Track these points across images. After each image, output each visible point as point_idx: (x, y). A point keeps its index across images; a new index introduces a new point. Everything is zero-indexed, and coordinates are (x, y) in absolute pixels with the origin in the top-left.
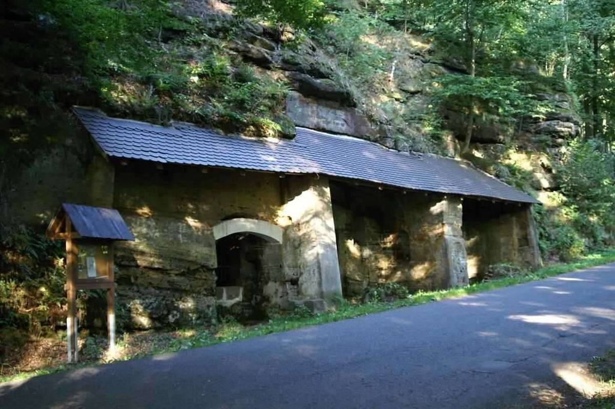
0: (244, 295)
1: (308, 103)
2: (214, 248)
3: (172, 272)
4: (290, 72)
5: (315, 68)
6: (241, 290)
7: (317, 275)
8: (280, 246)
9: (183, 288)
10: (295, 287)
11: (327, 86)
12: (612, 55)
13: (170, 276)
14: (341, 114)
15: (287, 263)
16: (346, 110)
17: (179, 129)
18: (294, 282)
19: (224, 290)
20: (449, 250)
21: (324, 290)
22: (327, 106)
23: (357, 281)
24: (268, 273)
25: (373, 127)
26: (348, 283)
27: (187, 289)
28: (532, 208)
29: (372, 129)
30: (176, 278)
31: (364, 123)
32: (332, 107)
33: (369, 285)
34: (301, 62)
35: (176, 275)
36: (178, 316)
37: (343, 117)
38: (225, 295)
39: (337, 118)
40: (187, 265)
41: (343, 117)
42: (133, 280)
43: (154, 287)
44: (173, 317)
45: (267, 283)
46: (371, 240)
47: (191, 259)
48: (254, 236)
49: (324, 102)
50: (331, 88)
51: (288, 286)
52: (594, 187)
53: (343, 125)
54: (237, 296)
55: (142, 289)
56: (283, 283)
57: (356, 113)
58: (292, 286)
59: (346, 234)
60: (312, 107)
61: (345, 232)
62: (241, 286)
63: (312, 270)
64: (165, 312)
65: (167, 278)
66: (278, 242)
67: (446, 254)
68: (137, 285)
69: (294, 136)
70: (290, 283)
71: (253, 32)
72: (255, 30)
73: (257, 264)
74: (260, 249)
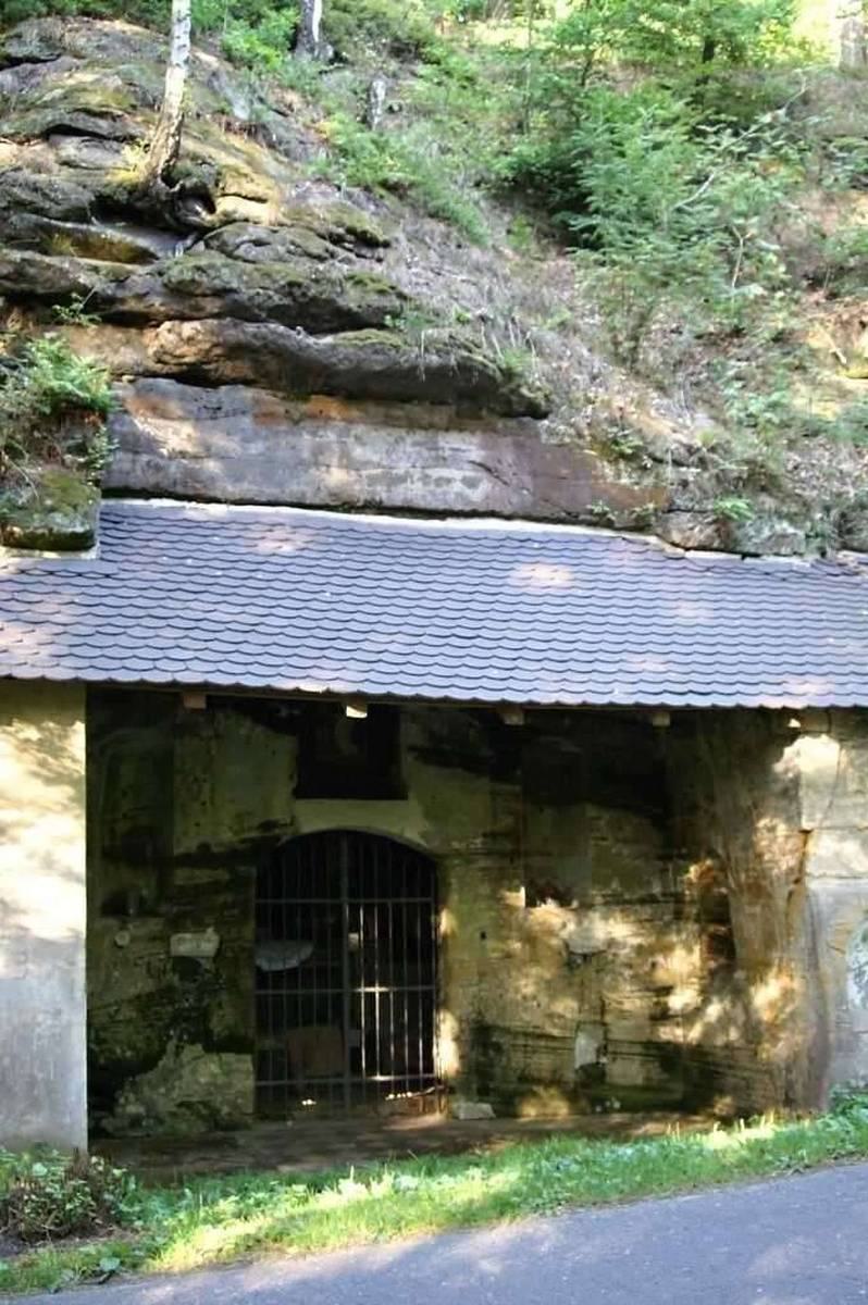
4: (197, 324)
5: (314, 299)
11: (362, 355)
12: (531, 961)
14: (468, 446)
16: (490, 429)
22: (389, 422)
23: (553, 1038)
25: (625, 481)
26: (498, 1048)
29: (624, 488)
31: (583, 468)
32: (412, 425)
33: (602, 1050)
34: (234, 285)
37: (476, 454)
39: (442, 461)
41: (476, 454)
46: (615, 885)
48: (604, 712)
49: (372, 408)
50: (380, 357)
53: (471, 483)
57: (544, 437)
59: (483, 869)
61: (483, 863)
71: (39, 211)
72: (47, 205)
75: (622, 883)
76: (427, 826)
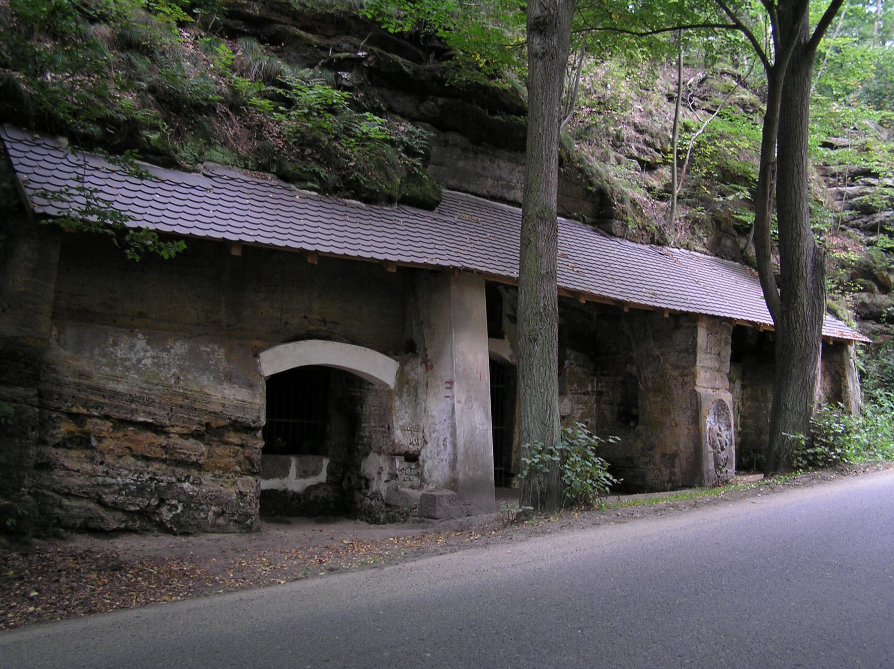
0: (330, 472)
1: (476, 153)
2: (262, 390)
3: (172, 430)
4: (445, 100)
6: (326, 462)
7: (449, 447)
8: (389, 393)
9: (194, 458)
10: (413, 466)
13: (170, 437)
15: (401, 423)
17: (210, 177)
18: (412, 458)
19: (294, 461)
20: (703, 412)
21: (461, 477)
24: (370, 437)
27: (201, 462)
28: (851, 349)
30: (180, 441)
35: (182, 435)
36: (180, 508)
38: (293, 470)
40: (205, 419)
42: (94, 443)
43: (134, 456)
44: (170, 510)
45: (367, 455)
47: (212, 408)
48: (350, 374)
51: (399, 463)
52: (226, 469)
54: (316, 473)
55: (109, 459)
56: (393, 455)
58: (406, 464)
60: (482, 160)
62: (326, 456)
63: (442, 438)
64: (154, 502)
65: (162, 440)
66: (388, 385)
67: (696, 419)
68: (101, 452)
69: (437, 203)
70: (403, 458)
73: (354, 422)
74: (359, 394)
75: (578, 385)
76: (510, 351)
